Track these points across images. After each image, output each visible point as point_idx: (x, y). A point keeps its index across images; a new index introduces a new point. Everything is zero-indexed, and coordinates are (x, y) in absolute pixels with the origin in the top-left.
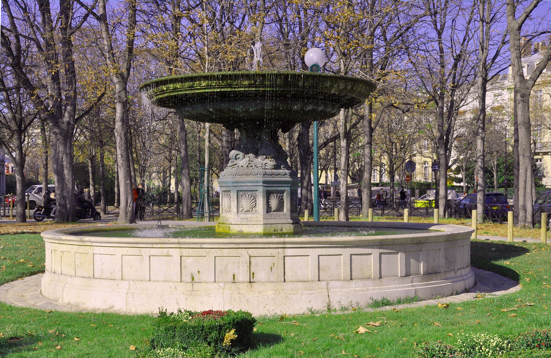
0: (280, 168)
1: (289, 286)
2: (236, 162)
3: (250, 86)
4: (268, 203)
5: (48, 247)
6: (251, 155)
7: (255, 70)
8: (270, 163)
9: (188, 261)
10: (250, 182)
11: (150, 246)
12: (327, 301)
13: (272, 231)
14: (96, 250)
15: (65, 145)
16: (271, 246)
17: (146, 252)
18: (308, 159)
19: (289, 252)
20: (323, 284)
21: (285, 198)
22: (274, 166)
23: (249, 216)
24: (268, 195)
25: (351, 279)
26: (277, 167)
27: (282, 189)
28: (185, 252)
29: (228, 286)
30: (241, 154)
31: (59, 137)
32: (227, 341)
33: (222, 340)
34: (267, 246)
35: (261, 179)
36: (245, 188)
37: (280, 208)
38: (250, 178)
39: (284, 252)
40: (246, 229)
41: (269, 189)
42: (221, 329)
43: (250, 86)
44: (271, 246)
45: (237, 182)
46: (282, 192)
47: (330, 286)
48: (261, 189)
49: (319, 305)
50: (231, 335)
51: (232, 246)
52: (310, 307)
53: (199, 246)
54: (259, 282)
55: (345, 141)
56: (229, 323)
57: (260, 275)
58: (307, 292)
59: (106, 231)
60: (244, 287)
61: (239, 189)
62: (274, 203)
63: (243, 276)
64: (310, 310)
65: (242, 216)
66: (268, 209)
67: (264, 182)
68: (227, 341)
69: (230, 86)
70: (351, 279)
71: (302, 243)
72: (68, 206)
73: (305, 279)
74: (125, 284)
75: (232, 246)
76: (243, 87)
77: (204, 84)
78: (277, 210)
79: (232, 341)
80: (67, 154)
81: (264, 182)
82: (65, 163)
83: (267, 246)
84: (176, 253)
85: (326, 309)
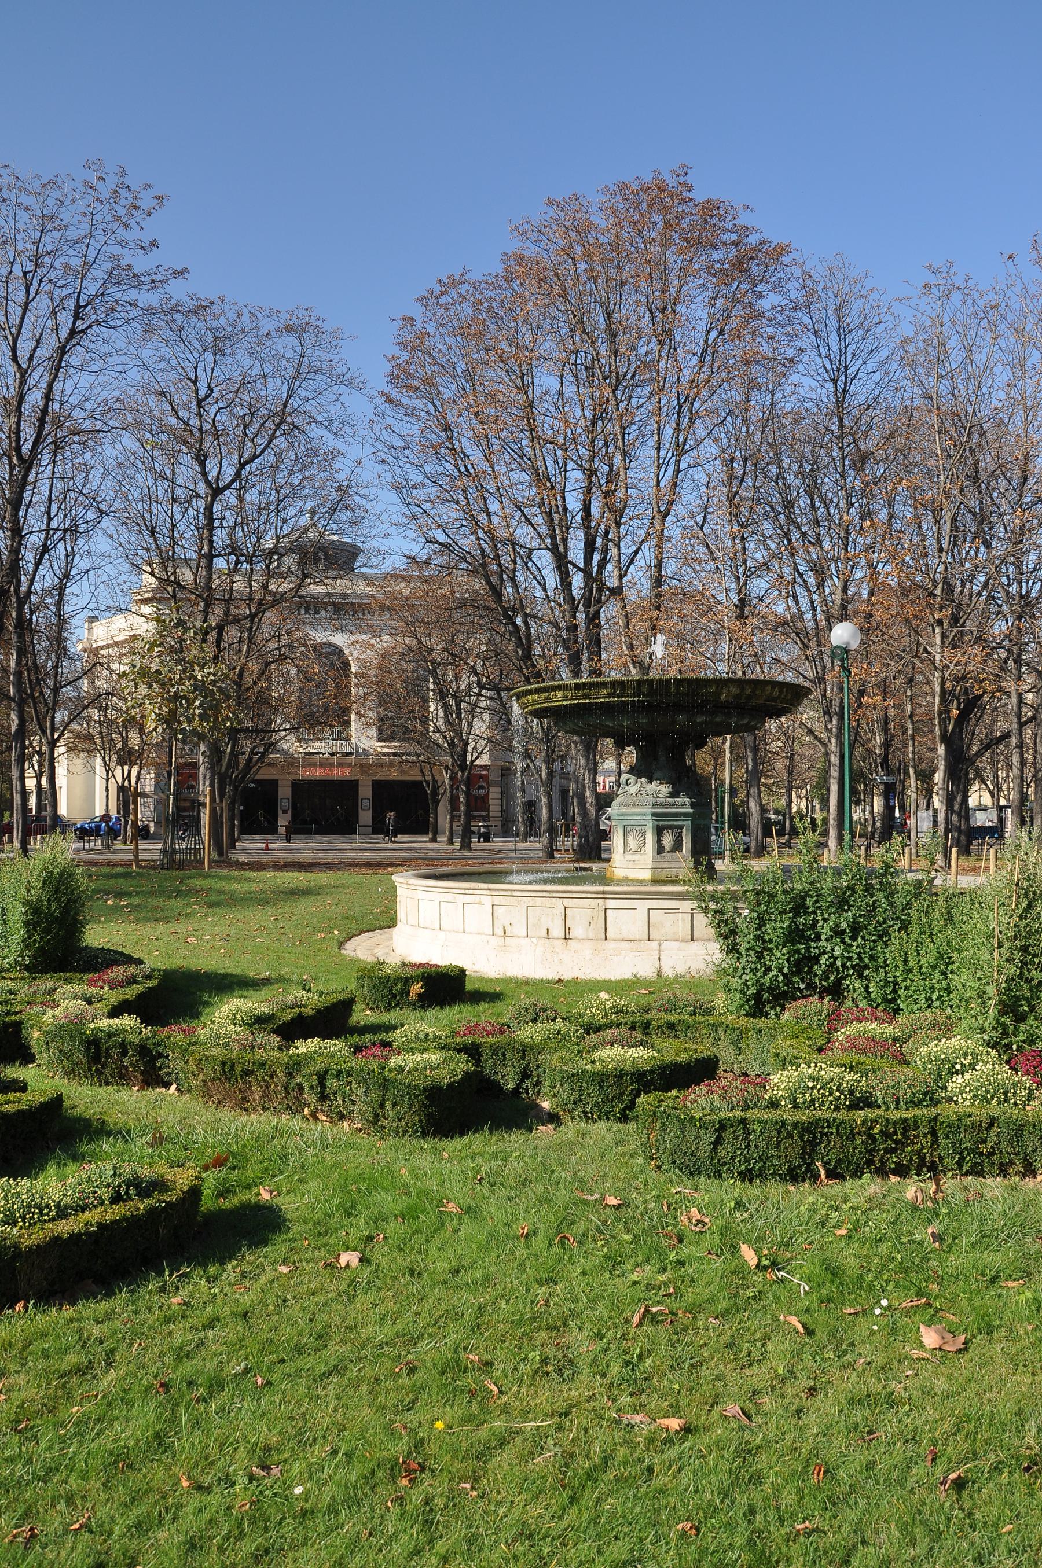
0: (678, 797)
1: (610, 945)
2: (627, 789)
3: (609, 696)
4: (659, 841)
5: (400, 891)
6: (643, 780)
7: (615, 675)
8: (664, 789)
9: (499, 911)
10: (637, 815)
11: (463, 891)
12: (657, 966)
13: (663, 877)
14: (421, 895)
15: (587, 759)
16: (589, 896)
17: (462, 899)
18: (962, 769)
19: (611, 904)
20: (654, 945)
21: (684, 835)
22: (670, 793)
23: (636, 857)
24: (659, 831)
25: (692, 939)
26: (672, 795)
27: (680, 823)
28: (497, 900)
29: (542, 941)
30: (633, 779)
31: (580, 747)
32: (413, 996)
33: (408, 993)
34: (583, 895)
35: (649, 811)
36: (632, 822)
37: (677, 846)
38: (637, 810)
39: (605, 904)
40: (632, 875)
41: (661, 823)
42: (407, 981)
43: (609, 696)
44: (589, 896)
45: (622, 815)
46: (681, 827)
47: (662, 947)
48: (650, 824)
49: (646, 970)
50: (417, 988)
51: (544, 894)
52: (635, 972)
53: (509, 893)
54: (576, 938)
55: (943, 747)
56: (418, 976)
57: (577, 931)
58: (633, 953)
59: (480, 874)
60: (559, 944)
61: (626, 823)
62: (668, 841)
63: (558, 932)
64: (635, 976)
65: (628, 857)
66: (660, 849)
67: (653, 815)
68: (413, 996)
69: (587, 696)
70: (692, 939)
71: (625, 893)
72: (591, 839)
73: (632, 938)
74: (442, 934)
75: (544, 894)
76: (602, 697)
77: (559, 695)
78: (673, 851)
79: (419, 995)
80: (589, 770)
81: (653, 815)
82: (587, 782)
83: (583, 895)
84: (487, 901)
85: (655, 975)
